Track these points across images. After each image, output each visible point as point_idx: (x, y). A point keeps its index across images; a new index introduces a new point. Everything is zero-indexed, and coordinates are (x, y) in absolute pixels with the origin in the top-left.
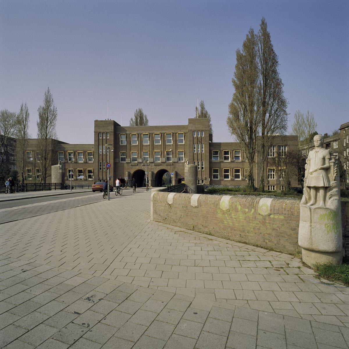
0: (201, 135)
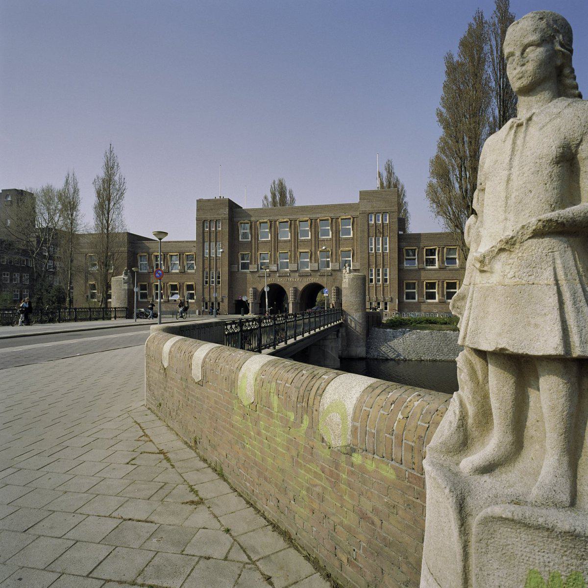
0: (375, 220)
